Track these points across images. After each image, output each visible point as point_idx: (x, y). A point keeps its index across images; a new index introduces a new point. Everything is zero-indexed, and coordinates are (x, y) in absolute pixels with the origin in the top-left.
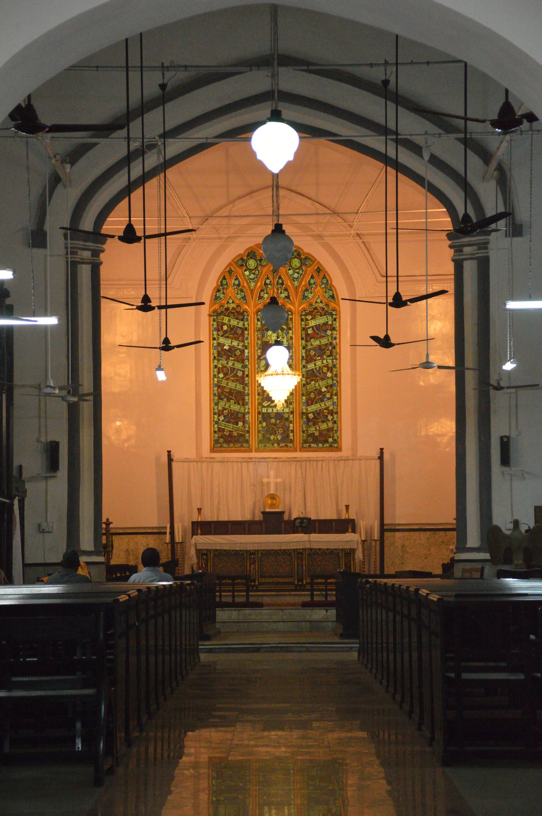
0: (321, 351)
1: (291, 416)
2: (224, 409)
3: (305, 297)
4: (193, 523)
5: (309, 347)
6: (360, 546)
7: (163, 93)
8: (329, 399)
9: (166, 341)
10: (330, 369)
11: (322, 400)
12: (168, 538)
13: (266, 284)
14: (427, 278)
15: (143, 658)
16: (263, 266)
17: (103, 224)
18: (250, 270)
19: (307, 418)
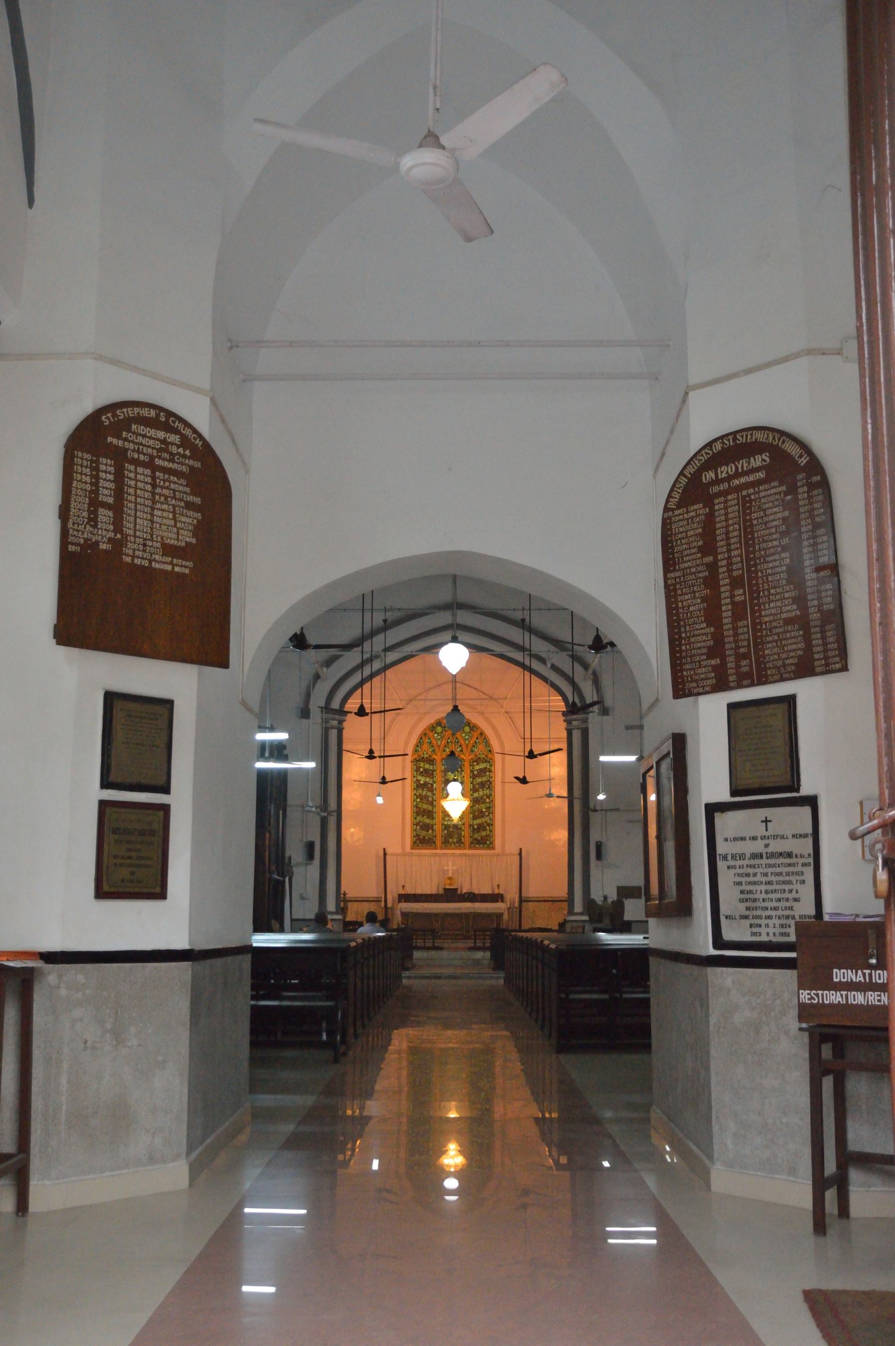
0: (482, 785)
1: (463, 826)
2: (420, 822)
3: (472, 751)
4: (399, 895)
5: (475, 783)
6: (506, 910)
7: (385, 625)
8: (487, 816)
9: (384, 778)
10: (488, 797)
11: (483, 817)
12: (383, 904)
13: (448, 742)
14: (550, 740)
15: (365, 982)
16: (446, 731)
17: (345, 704)
18: (438, 734)
19: (473, 828)
